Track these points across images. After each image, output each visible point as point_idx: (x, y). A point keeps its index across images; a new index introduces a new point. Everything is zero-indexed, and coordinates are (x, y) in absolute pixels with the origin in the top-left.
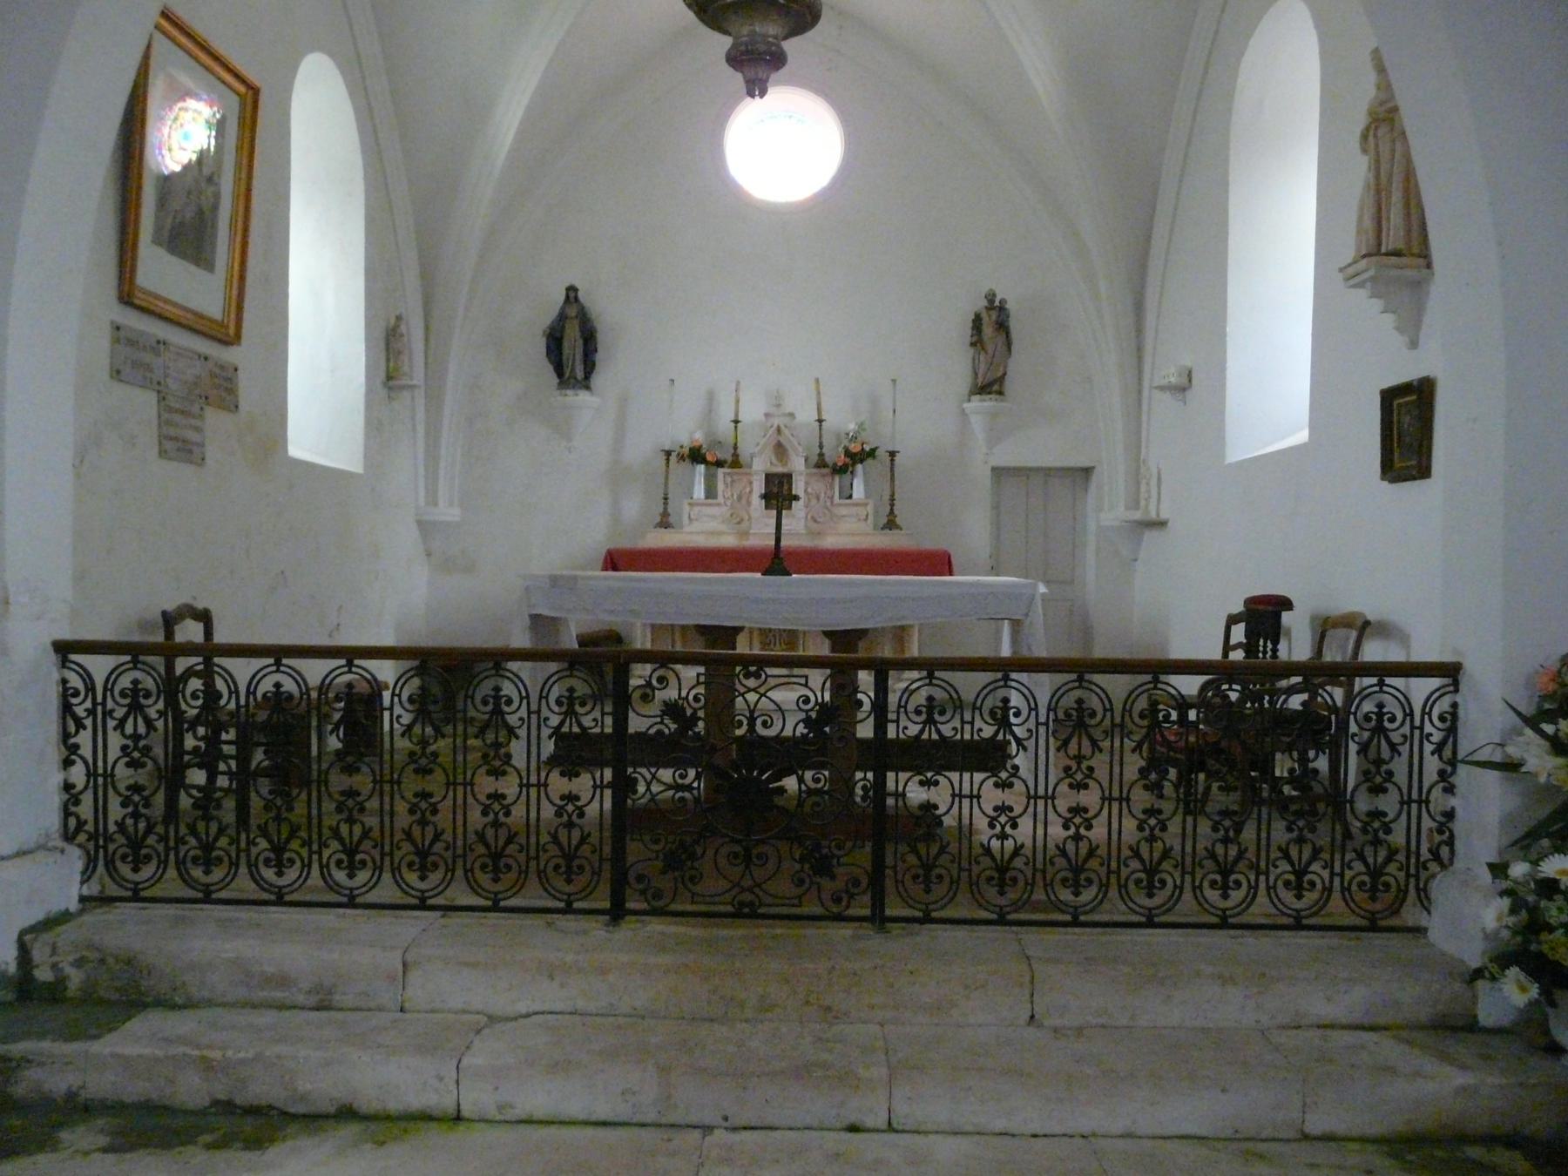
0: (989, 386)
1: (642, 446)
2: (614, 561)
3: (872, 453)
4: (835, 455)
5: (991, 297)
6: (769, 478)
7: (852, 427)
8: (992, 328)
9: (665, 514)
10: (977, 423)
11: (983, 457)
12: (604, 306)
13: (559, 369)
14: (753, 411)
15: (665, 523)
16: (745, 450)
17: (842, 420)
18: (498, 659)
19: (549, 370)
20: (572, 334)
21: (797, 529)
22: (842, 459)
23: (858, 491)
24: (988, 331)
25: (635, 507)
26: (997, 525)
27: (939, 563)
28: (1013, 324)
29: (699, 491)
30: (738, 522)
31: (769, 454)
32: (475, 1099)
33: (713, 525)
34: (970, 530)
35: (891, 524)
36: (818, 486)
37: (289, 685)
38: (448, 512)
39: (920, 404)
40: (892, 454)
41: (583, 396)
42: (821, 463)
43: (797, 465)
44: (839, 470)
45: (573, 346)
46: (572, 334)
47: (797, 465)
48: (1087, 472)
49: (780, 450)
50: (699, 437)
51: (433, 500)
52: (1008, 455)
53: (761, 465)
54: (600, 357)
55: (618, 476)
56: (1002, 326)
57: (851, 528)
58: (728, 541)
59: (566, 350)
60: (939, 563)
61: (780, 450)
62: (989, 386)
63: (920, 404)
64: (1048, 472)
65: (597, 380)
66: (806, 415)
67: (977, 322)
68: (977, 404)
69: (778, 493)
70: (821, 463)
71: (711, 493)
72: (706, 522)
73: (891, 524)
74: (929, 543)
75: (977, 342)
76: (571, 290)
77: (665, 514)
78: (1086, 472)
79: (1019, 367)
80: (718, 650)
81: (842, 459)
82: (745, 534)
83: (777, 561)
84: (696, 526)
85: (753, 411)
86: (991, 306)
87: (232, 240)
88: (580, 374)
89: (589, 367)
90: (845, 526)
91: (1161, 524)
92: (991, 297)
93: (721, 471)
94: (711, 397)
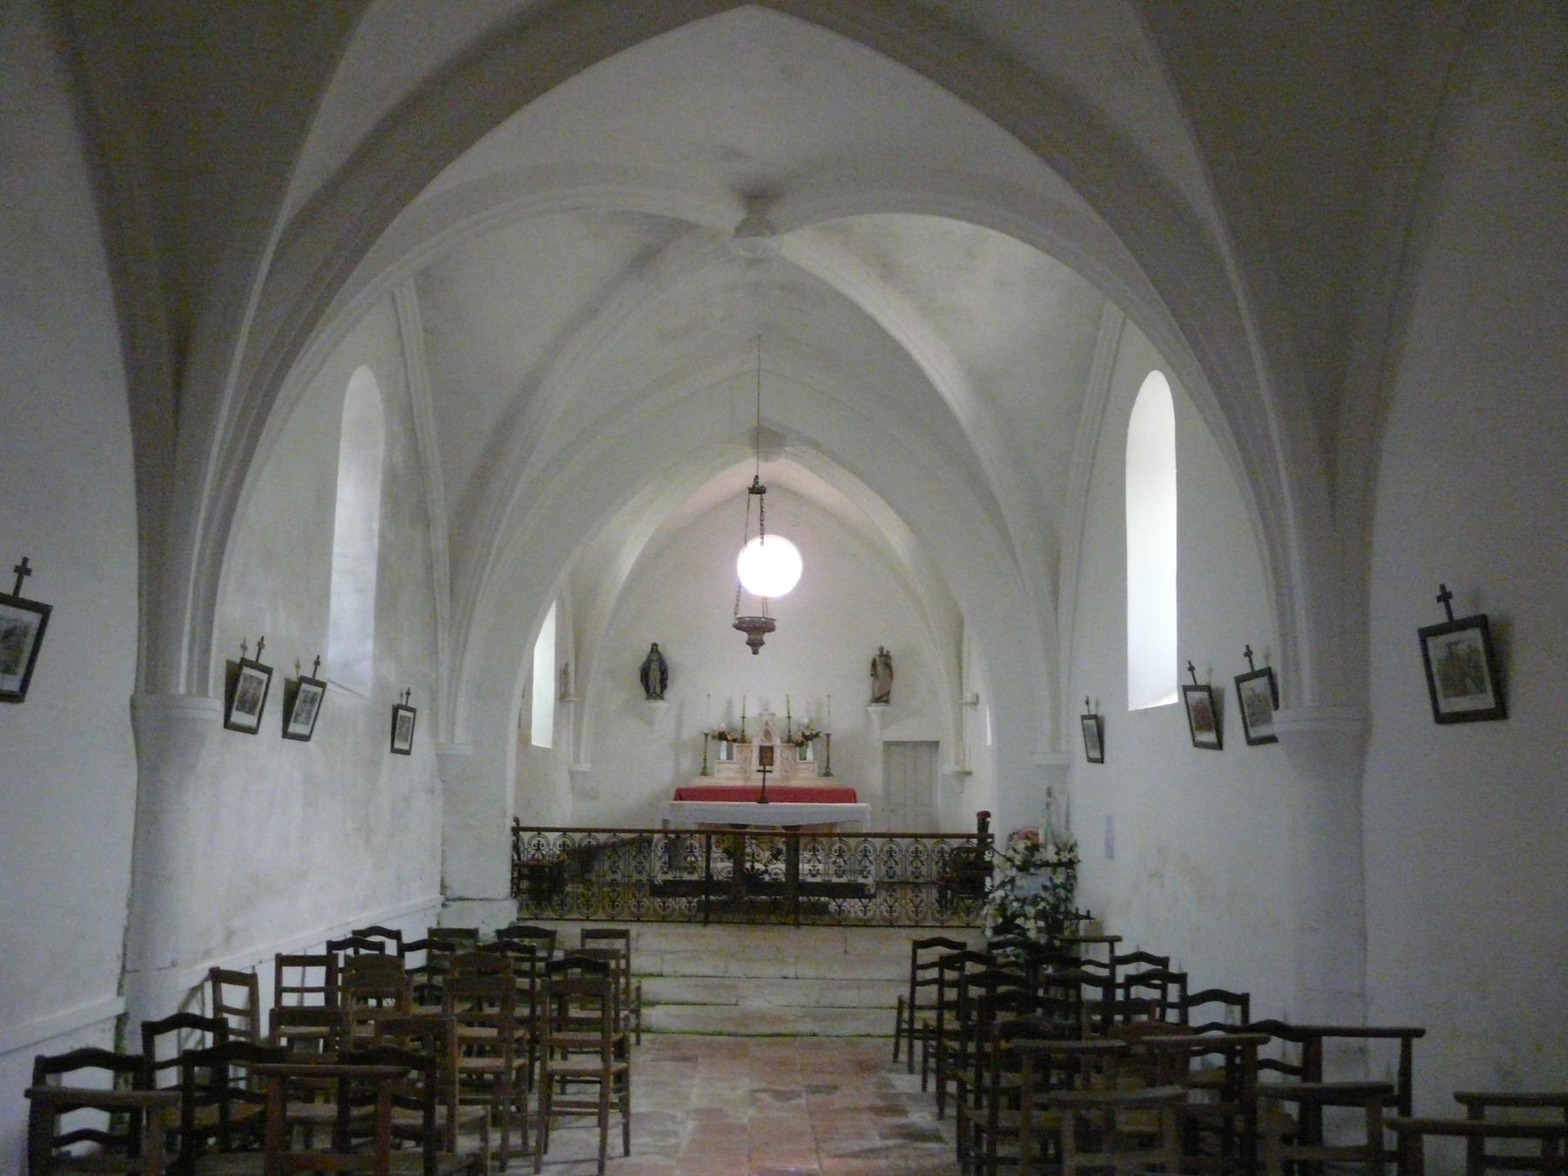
0: (881, 698)
1: (692, 731)
2: (681, 795)
3: (817, 735)
4: (798, 737)
5: (881, 649)
6: (762, 749)
7: (806, 721)
8: (882, 666)
9: (705, 768)
10: (874, 717)
11: (878, 737)
12: (672, 654)
13: (647, 690)
14: (753, 711)
15: (704, 773)
16: (748, 732)
17: (801, 716)
18: (653, 832)
19: (642, 690)
20: (655, 666)
21: (775, 778)
22: (801, 739)
23: (810, 755)
24: (880, 668)
25: (687, 764)
26: (887, 772)
27: (849, 796)
28: (894, 664)
29: (723, 756)
30: (744, 771)
31: (761, 736)
32: (667, 969)
33: (732, 774)
34: (871, 777)
35: (828, 774)
36: (788, 753)
37: (569, 842)
38: (585, 766)
39: (846, 710)
40: (828, 736)
41: (660, 703)
42: (789, 740)
43: (776, 741)
44: (800, 745)
45: (655, 676)
46: (655, 666)
47: (776, 741)
48: (937, 743)
49: (767, 734)
50: (723, 727)
51: (577, 759)
52: (893, 734)
53: (757, 742)
54: (669, 682)
55: (678, 746)
56: (888, 666)
57: (806, 777)
58: (739, 783)
59: (651, 679)
60: (849, 796)
61: (767, 734)
62: (881, 698)
63: (846, 710)
64: (917, 744)
65: (668, 694)
66: (781, 713)
67: (874, 664)
68: (875, 709)
69: (766, 755)
70: (789, 740)
71: (730, 757)
72: (727, 773)
73: (828, 774)
74: (848, 785)
75: (874, 674)
76: (655, 645)
77: (705, 768)
78: (936, 743)
79: (898, 688)
80: (735, 838)
81: (801, 739)
82: (747, 779)
83: (762, 795)
84: (721, 775)
85: (753, 711)
86: (882, 655)
87: (222, 475)
88: (658, 690)
89: (664, 686)
90: (802, 775)
91: (969, 774)
92: (881, 649)
93: (735, 745)
94: (730, 703)
